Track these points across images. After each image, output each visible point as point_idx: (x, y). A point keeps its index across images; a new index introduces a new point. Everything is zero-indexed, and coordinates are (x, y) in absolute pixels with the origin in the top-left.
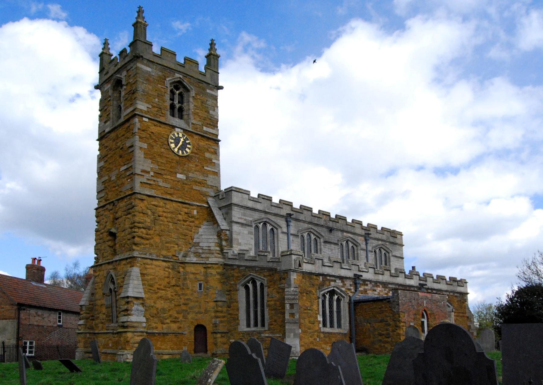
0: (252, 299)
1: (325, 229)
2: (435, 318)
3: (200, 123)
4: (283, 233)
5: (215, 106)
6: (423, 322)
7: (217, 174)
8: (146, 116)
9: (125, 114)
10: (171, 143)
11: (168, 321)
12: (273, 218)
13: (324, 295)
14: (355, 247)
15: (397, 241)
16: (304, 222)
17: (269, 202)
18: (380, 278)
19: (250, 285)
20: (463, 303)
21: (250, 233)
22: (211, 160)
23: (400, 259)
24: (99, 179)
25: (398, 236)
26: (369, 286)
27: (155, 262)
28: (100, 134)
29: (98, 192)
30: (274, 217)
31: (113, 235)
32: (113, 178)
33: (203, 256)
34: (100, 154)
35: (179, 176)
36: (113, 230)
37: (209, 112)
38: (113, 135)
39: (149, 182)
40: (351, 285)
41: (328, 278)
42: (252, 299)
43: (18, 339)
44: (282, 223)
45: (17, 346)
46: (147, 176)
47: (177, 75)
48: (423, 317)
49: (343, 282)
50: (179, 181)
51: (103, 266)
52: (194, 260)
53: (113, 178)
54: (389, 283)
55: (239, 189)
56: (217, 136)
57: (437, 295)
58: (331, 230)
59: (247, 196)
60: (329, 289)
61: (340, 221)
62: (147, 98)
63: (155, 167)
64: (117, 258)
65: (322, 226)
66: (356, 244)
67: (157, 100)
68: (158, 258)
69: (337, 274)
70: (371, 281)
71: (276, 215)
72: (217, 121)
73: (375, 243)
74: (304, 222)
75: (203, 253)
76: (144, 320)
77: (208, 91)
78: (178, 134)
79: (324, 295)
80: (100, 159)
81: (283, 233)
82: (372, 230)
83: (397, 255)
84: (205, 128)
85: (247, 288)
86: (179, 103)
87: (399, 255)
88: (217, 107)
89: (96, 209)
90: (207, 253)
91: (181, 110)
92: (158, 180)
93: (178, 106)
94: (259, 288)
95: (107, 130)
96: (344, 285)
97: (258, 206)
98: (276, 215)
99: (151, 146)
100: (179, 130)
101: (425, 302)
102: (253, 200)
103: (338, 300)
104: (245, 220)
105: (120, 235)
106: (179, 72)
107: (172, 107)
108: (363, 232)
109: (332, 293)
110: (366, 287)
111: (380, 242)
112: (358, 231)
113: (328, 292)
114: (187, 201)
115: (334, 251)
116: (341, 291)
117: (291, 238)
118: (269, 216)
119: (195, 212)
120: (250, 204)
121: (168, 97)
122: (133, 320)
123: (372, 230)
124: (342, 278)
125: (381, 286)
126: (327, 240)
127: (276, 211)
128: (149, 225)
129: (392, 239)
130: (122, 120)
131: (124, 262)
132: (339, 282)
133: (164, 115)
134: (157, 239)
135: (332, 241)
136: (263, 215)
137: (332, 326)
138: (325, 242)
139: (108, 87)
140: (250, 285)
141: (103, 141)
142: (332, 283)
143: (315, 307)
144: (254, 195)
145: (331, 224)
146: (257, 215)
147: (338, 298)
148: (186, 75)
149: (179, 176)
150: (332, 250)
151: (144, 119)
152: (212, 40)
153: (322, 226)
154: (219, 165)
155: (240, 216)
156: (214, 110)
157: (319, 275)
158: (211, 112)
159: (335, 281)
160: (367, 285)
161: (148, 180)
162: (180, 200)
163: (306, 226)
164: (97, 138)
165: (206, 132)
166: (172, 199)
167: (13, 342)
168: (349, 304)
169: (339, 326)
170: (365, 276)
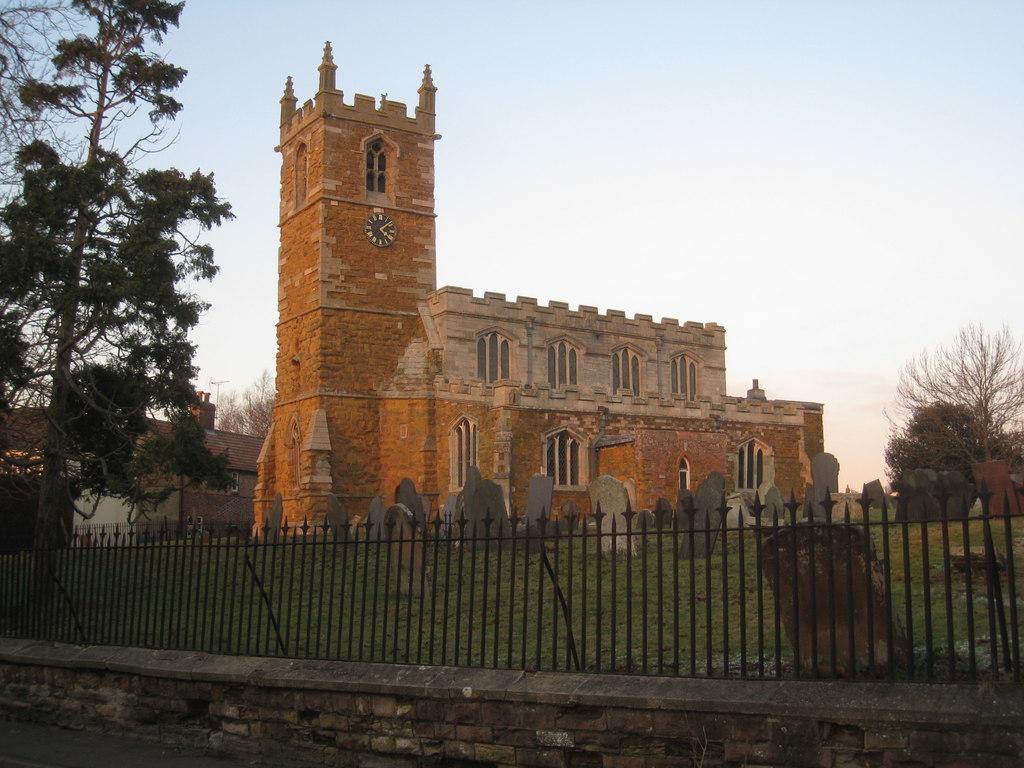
0: (464, 447)
1: (588, 335)
2: (703, 468)
3: (406, 195)
4: (521, 346)
5: (430, 166)
6: (683, 475)
7: (431, 266)
8: (334, 198)
9: (311, 194)
10: (368, 231)
11: (363, 481)
12: (506, 326)
13: (551, 439)
14: (639, 357)
15: (714, 342)
16: (554, 326)
17: (500, 302)
18: (642, 410)
19: (463, 428)
20: (794, 441)
21: (471, 351)
22: (422, 246)
23: (719, 372)
24: (281, 282)
25: (717, 334)
26: (623, 423)
27: (345, 401)
28: (281, 218)
29: (280, 302)
30: (507, 324)
31: (296, 363)
32: (297, 284)
33: (408, 388)
34: (282, 247)
35: (379, 276)
36: (297, 358)
37: (418, 176)
38: (296, 221)
39: (339, 290)
40: (593, 423)
41: (558, 414)
42: (464, 447)
43: (182, 514)
44: (522, 332)
45: (181, 521)
46: (337, 282)
47: (376, 131)
48: (683, 465)
49: (580, 419)
50: (379, 282)
51: (285, 407)
52: (397, 394)
53: (297, 284)
54: (656, 418)
55: (458, 288)
56: (432, 209)
57: (708, 435)
58: (598, 335)
59: (468, 298)
60: (558, 431)
61: (614, 319)
62: (337, 172)
63: (346, 267)
64: (299, 398)
65: (583, 330)
66: (640, 352)
67: (348, 172)
68: (350, 395)
69: (571, 409)
70: (625, 417)
71: (510, 320)
72: (431, 188)
73: (676, 348)
74: (554, 326)
75: (408, 384)
76: (329, 479)
77: (420, 145)
78: (377, 216)
79: (551, 439)
80: (283, 253)
81: (521, 346)
82: (669, 327)
83: (713, 365)
84: (414, 201)
85: (459, 431)
86: (380, 169)
87: (717, 365)
88: (433, 166)
89: (277, 326)
90: (414, 384)
91: (382, 179)
92: (351, 285)
93: (377, 175)
94: (472, 431)
95: (290, 214)
96: (582, 424)
97: (485, 311)
98: (510, 320)
99: (340, 240)
100: (379, 210)
101: (686, 445)
102: (478, 301)
103: (574, 446)
104: (465, 332)
105: (305, 364)
106: (379, 126)
107: (370, 177)
108: (653, 333)
109: (564, 435)
110: (618, 425)
111: (683, 347)
112: (644, 331)
113: (558, 434)
114: (388, 311)
115: (602, 367)
116: (579, 432)
117: (534, 352)
118: (500, 324)
119: (400, 326)
120: (473, 309)
121: (363, 166)
122: (318, 481)
123: (669, 327)
124: (578, 414)
125: (642, 422)
126: (591, 351)
127: (511, 314)
128: (339, 349)
129: (703, 340)
130: (307, 203)
131: (308, 402)
132: (575, 420)
133: (358, 192)
134: (350, 369)
135: (599, 352)
136: (491, 323)
137: (563, 481)
138: (588, 354)
139: (291, 151)
140: (463, 428)
141: (286, 227)
142: (564, 423)
143: (536, 456)
144: (479, 294)
145: (597, 326)
146: (481, 325)
147: (574, 442)
148: (387, 129)
149: (379, 276)
150: (598, 365)
151: (333, 203)
152: (428, 66)
153: (583, 330)
154: (434, 253)
155: (457, 329)
156: (428, 172)
157: (543, 412)
158: (423, 176)
159: (568, 419)
160: (619, 421)
161: (337, 287)
162: (381, 311)
163: (558, 332)
164: (278, 223)
165: (417, 207)
166: (369, 309)
167: (175, 518)
168: (589, 449)
169: (574, 481)
170: (614, 408)
